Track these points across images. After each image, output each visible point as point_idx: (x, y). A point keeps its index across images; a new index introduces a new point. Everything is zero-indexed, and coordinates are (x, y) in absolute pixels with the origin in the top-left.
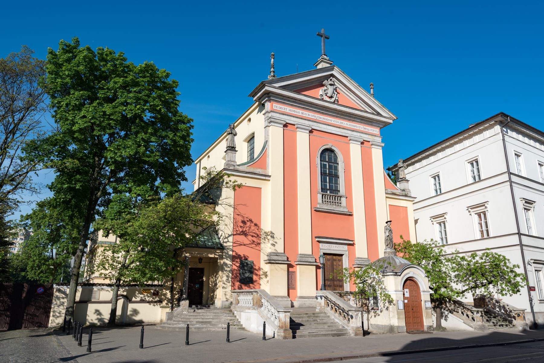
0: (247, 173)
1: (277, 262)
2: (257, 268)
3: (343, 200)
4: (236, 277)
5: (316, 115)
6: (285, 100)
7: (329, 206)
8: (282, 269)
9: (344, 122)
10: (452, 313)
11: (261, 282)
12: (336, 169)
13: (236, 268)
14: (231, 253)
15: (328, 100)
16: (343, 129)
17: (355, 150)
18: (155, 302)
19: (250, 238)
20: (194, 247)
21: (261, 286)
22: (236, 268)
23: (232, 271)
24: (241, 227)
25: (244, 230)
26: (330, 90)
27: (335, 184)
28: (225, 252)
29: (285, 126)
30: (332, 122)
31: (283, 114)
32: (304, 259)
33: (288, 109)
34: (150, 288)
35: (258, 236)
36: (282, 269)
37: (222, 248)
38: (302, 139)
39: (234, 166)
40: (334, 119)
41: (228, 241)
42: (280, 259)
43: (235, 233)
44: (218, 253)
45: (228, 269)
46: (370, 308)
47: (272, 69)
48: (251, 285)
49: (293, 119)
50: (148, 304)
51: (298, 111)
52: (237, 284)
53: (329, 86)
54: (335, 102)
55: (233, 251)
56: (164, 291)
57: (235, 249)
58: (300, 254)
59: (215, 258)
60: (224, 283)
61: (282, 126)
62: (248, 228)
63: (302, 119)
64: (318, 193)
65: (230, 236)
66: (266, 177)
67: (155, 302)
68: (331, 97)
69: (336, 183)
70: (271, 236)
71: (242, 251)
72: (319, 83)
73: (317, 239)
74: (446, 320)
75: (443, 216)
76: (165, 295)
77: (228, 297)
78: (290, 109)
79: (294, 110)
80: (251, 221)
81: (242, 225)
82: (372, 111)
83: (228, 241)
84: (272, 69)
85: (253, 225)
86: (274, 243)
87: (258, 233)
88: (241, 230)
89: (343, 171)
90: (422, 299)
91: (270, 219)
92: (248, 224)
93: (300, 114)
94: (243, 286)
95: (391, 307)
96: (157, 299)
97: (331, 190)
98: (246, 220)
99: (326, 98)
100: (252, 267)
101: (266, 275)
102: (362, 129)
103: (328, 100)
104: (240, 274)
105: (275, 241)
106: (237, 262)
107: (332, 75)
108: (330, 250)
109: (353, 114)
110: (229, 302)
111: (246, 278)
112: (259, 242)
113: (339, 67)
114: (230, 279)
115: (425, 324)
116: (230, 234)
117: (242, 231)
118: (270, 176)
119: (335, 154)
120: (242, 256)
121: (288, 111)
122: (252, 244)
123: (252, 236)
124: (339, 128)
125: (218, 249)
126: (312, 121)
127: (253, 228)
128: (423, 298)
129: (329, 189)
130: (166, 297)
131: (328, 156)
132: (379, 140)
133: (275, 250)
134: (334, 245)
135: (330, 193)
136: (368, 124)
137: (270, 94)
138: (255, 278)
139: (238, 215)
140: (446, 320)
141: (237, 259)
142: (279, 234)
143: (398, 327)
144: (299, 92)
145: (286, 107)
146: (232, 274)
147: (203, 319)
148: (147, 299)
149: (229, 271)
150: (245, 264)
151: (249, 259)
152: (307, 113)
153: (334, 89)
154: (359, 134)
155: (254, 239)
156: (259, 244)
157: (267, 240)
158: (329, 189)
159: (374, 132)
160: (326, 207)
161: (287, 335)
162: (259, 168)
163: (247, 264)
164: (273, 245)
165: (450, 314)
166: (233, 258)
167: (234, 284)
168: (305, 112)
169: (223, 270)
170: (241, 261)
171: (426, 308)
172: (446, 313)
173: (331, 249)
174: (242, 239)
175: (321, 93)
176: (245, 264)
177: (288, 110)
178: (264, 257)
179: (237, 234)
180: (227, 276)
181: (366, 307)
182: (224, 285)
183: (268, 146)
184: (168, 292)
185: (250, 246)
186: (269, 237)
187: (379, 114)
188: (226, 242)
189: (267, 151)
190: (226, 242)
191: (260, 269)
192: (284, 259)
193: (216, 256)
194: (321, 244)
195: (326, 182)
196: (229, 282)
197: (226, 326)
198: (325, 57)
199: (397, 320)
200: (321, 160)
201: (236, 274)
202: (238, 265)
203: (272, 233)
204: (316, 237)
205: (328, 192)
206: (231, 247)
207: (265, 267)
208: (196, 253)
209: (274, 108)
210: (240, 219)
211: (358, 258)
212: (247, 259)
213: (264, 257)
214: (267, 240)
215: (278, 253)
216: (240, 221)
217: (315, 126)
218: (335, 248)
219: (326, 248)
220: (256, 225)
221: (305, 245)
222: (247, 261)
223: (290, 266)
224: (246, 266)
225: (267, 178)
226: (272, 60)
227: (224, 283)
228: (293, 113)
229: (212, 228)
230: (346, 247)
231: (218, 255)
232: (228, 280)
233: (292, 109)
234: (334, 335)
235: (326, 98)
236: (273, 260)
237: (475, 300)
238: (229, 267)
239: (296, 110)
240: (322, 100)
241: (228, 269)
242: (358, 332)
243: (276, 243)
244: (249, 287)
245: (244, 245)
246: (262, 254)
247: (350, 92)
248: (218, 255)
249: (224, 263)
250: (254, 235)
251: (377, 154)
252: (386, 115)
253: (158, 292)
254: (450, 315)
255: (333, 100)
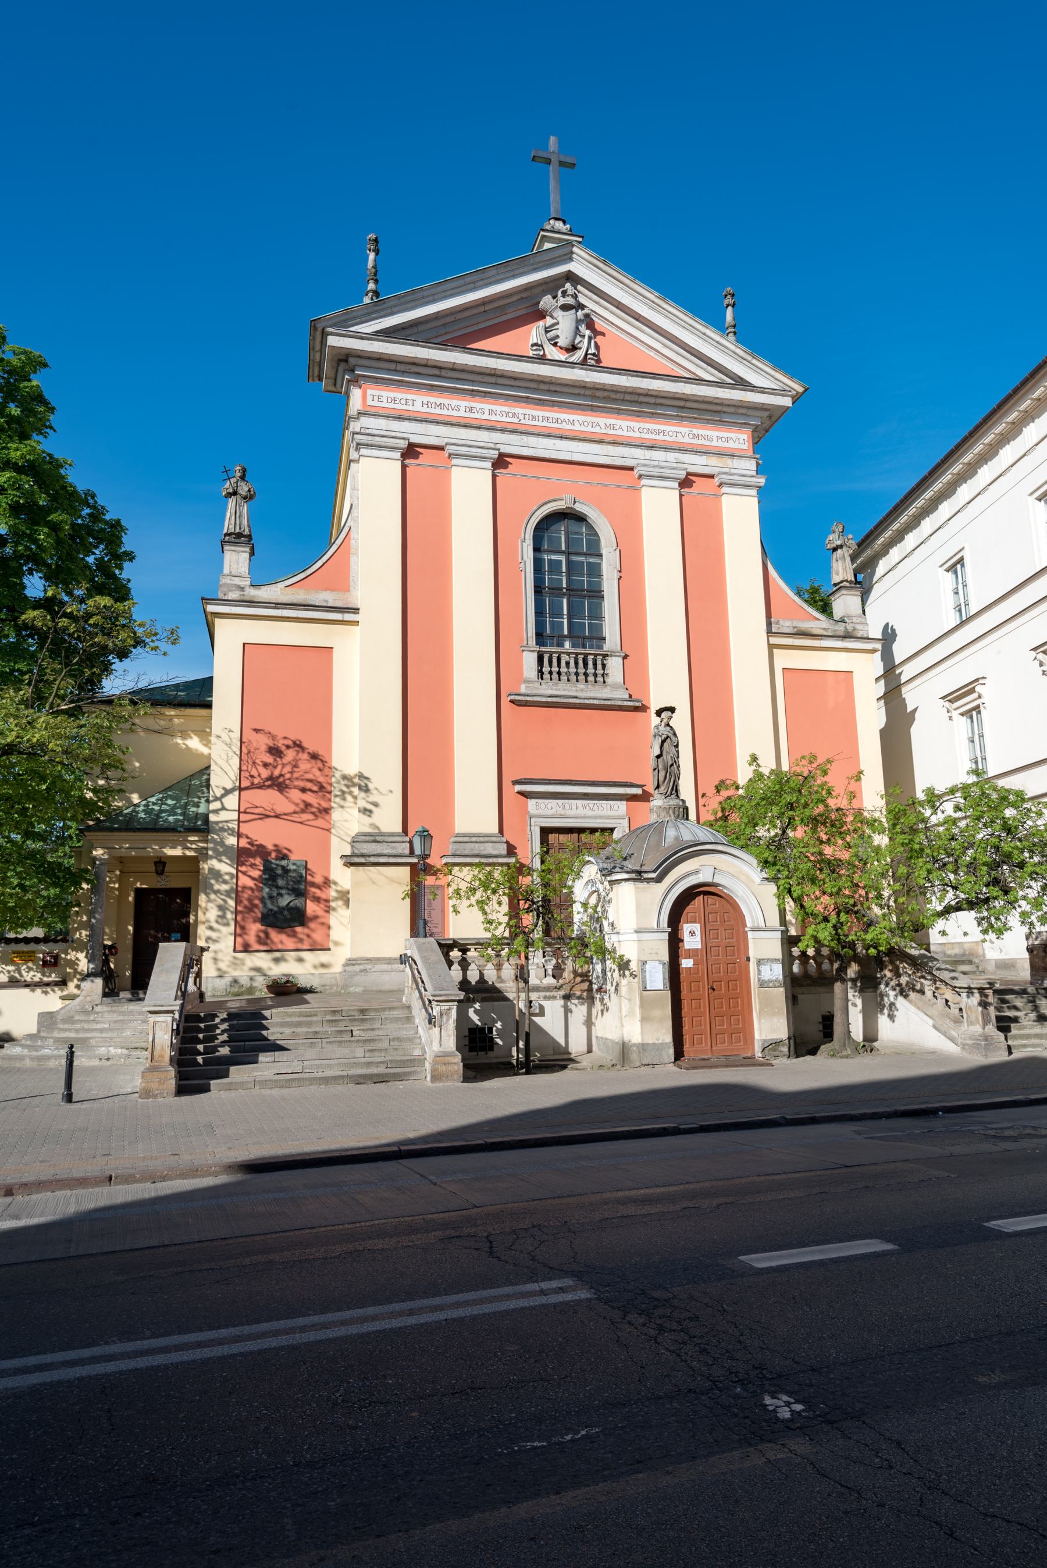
0: (278, 605)
1: (373, 860)
2: (318, 879)
3: (614, 665)
4: (250, 909)
5: (518, 410)
6: (403, 373)
7: (560, 685)
8: (392, 880)
9: (618, 422)
10: (906, 996)
11: (333, 919)
12: (595, 571)
13: (250, 883)
14: (232, 841)
15: (562, 356)
16: (615, 443)
17: (659, 508)
18: (48, 984)
19: (295, 795)
20: (118, 830)
21: (331, 932)
22: (250, 883)
23: (237, 893)
24: (266, 765)
25: (277, 773)
26: (565, 324)
27: (590, 618)
28: (213, 841)
29: (686, 482)
30: (577, 427)
31: (400, 418)
32: (468, 849)
33: (418, 401)
34: (32, 947)
35: (322, 787)
36: (392, 880)
37: (202, 827)
38: (469, 489)
39: (242, 589)
40: (581, 418)
41: (223, 808)
42: (385, 852)
43: (245, 783)
44: (192, 842)
45: (225, 887)
46: (595, 987)
47: (371, 286)
48: (298, 929)
49: (702, 460)
50: (27, 991)
51: (454, 403)
52: (254, 928)
53: (559, 314)
54: (593, 361)
55: (239, 836)
56: (72, 955)
57: (245, 829)
58: (458, 835)
59: (184, 858)
60: (211, 928)
61: (676, 485)
62: (293, 767)
63: (465, 426)
64: (525, 648)
65: (227, 792)
66: (345, 613)
67: (48, 984)
68: (573, 348)
69: (597, 614)
70: (360, 788)
71: (267, 834)
72: (526, 309)
73: (518, 788)
74: (891, 1017)
75: (973, 691)
76: (73, 964)
77: (223, 966)
78: (426, 399)
79: (439, 401)
80: (298, 746)
81: (269, 759)
82: (717, 376)
83: (223, 808)
84: (371, 286)
85: (305, 756)
86: (370, 807)
87: (321, 779)
88: (265, 773)
89: (616, 575)
90: (752, 954)
91: (361, 735)
92: (290, 755)
93: (486, 416)
94: (274, 934)
95: (624, 982)
96: (54, 977)
97: (577, 636)
98: (281, 744)
99: (552, 353)
100: (301, 879)
101: (344, 897)
102: (687, 440)
103: (562, 356)
104: (262, 900)
105: (372, 799)
106: (252, 865)
107: (571, 277)
108: (561, 817)
109: (647, 394)
110: (227, 980)
111: (282, 910)
112: (324, 805)
113: (587, 243)
114: (230, 916)
115: (757, 1036)
116: (229, 786)
117: (270, 778)
118: (356, 610)
119: (590, 527)
120: (270, 847)
121: (418, 407)
122: (303, 811)
123: (303, 790)
124: (601, 442)
125: (195, 830)
126: (503, 431)
127: (304, 766)
128: (754, 951)
129: (570, 636)
130: (75, 970)
131: (562, 534)
132: (749, 466)
133: (372, 825)
134: (579, 802)
135: (574, 646)
136: (708, 421)
137: (352, 361)
138: (311, 908)
139: (257, 731)
140: (891, 1017)
141: (253, 856)
142: (387, 778)
143: (643, 1047)
144: (461, 343)
145: (410, 397)
146: (238, 902)
147: (77, 1031)
148: (28, 977)
149: (228, 893)
150: (279, 872)
151: (293, 857)
152: (487, 407)
153: (578, 322)
154: (671, 456)
155: (309, 797)
156: (327, 811)
157: (349, 798)
158: (570, 636)
159: (731, 445)
160: (549, 689)
161: (154, 1086)
162: (326, 589)
163: (286, 871)
164: (367, 812)
165: (900, 998)
166: (241, 856)
167: (243, 928)
168: (477, 405)
169: (208, 889)
170: (267, 864)
171: (762, 984)
172: (892, 993)
173: (569, 813)
174: (269, 799)
175: (534, 339)
176: (279, 872)
177: (463, 409)
178: (339, 847)
179: (252, 787)
180: (221, 908)
181: (586, 985)
182: (209, 933)
183: (356, 521)
184: (81, 956)
185: (296, 818)
186: (356, 790)
187: (740, 383)
188: (216, 812)
189: (352, 534)
190: (216, 812)
191: (327, 882)
192: (399, 851)
193: (188, 853)
194: (532, 803)
195: (561, 616)
196: (227, 924)
197: (64, 1052)
198: (559, 225)
199: (639, 1024)
200: (537, 549)
201: (250, 900)
202: (256, 874)
203: (361, 776)
204: (516, 782)
205: (567, 644)
206: (234, 825)
207: (342, 876)
208: (126, 845)
209: (370, 402)
210: (262, 742)
211: (465, 835)
212: (285, 857)
213: (339, 847)
214: (349, 798)
215: (383, 835)
216: (263, 748)
217: (512, 444)
218: (581, 812)
219: (550, 813)
220: (314, 756)
221: (473, 807)
222: (284, 863)
223: (420, 869)
224: (282, 876)
225: (348, 617)
226: (372, 256)
227: (211, 928)
228: (438, 411)
229: (199, 779)
230: (621, 807)
231: (195, 850)
232: (223, 917)
233: (432, 399)
234: (359, 1080)
235: (552, 353)
236: (363, 856)
237: (1030, 950)
238: (225, 882)
239: (446, 401)
240: (542, 359)
241: (225, 887)
242: (442, 1069)
243: (376, 805)
244: (294, 935)
245: (277, 816)
246: (334, 841)
247: (646, 329)
248: (195, 850)
249: (211, 870)
250: (309, 785)
251: (740, 518)
252: (768, 384)
253: (56, 958)
254: (901, 1002)
255: (578, 356)
